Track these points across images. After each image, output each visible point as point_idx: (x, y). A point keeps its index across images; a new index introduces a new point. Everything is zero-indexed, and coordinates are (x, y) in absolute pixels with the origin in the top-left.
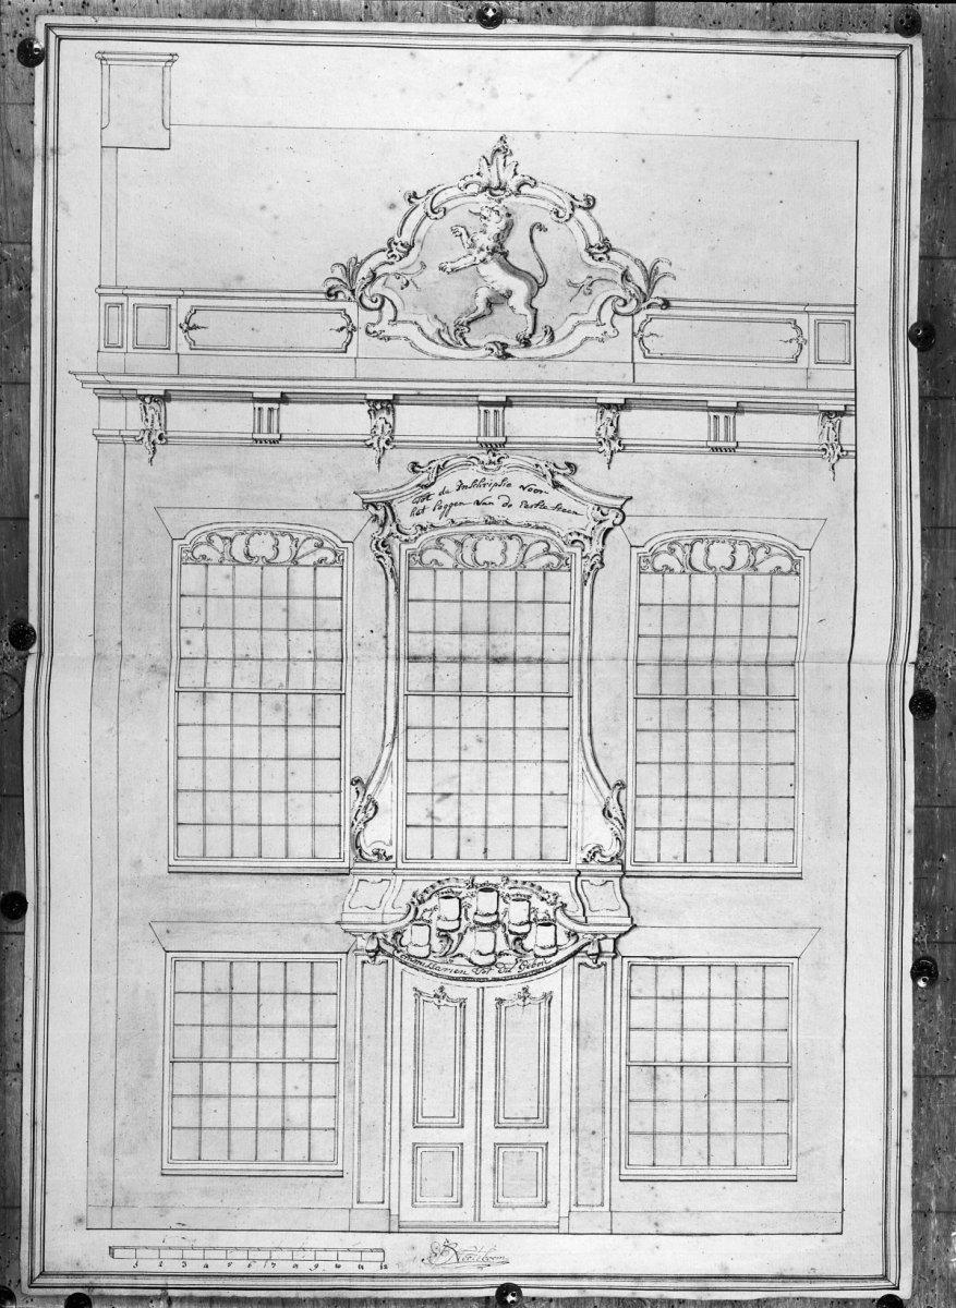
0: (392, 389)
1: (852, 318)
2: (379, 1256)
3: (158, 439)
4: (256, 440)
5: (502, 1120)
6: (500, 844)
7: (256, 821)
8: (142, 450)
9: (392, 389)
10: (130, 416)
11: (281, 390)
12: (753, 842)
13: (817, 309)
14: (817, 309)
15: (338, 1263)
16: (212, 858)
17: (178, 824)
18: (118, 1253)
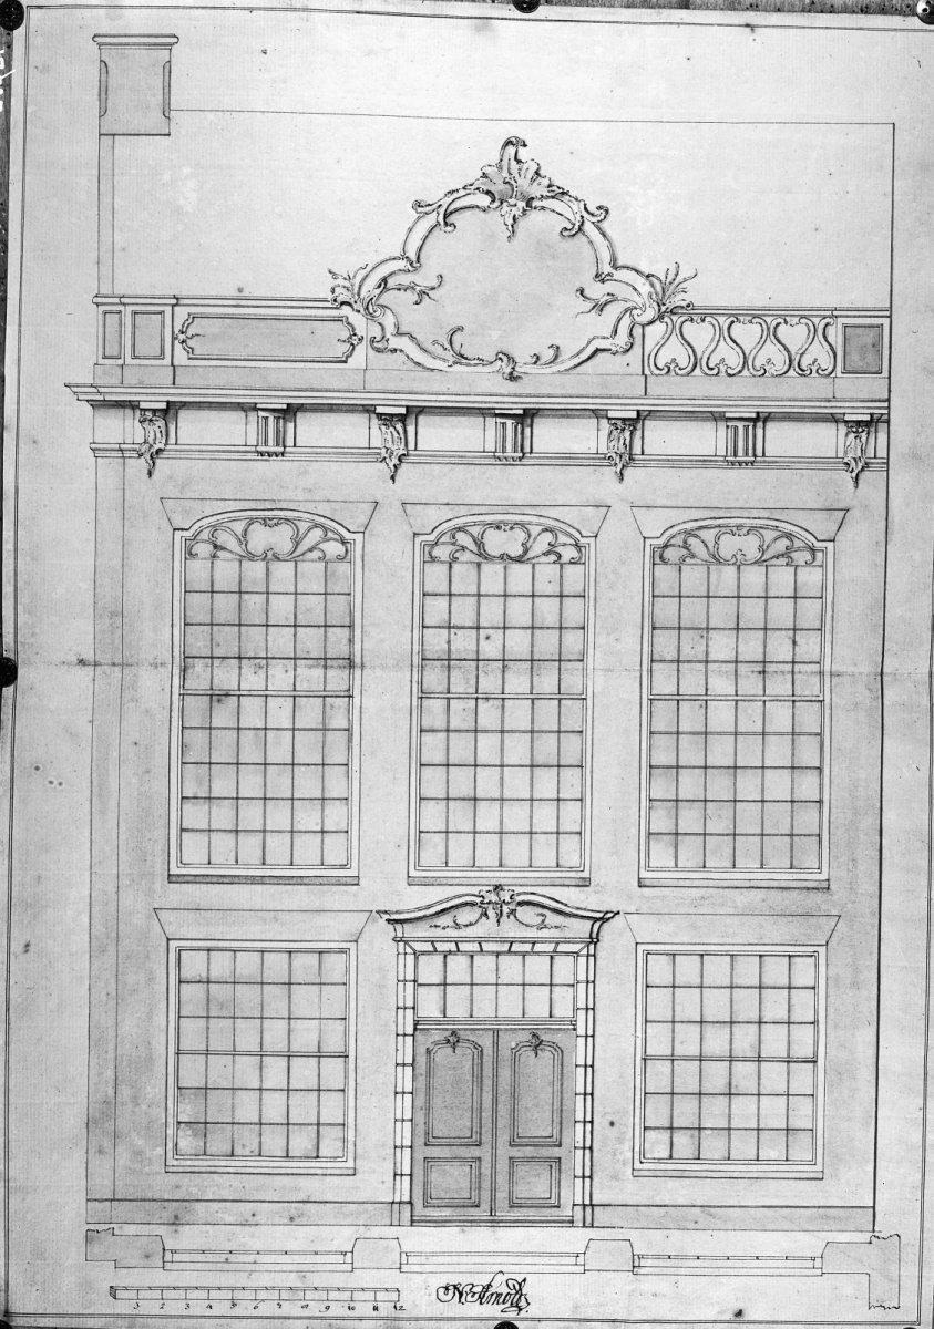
0: (636, 405)
1: (886, 322)
2: (394, 1296)
3: (628, 459)
4: (262, 454)
5: (517, 1140)
6: (517, 850)
7: (477, 829)
8: (138, 466)
9: (636, 405)
10: (121, 429)
11: (166, 399)
12: (278, 847)
13: (133, 301)
14: (133, 301)
15: (352, 1304)
16: (481, 869)
17: (182, 830)
18: (119, 1294)
